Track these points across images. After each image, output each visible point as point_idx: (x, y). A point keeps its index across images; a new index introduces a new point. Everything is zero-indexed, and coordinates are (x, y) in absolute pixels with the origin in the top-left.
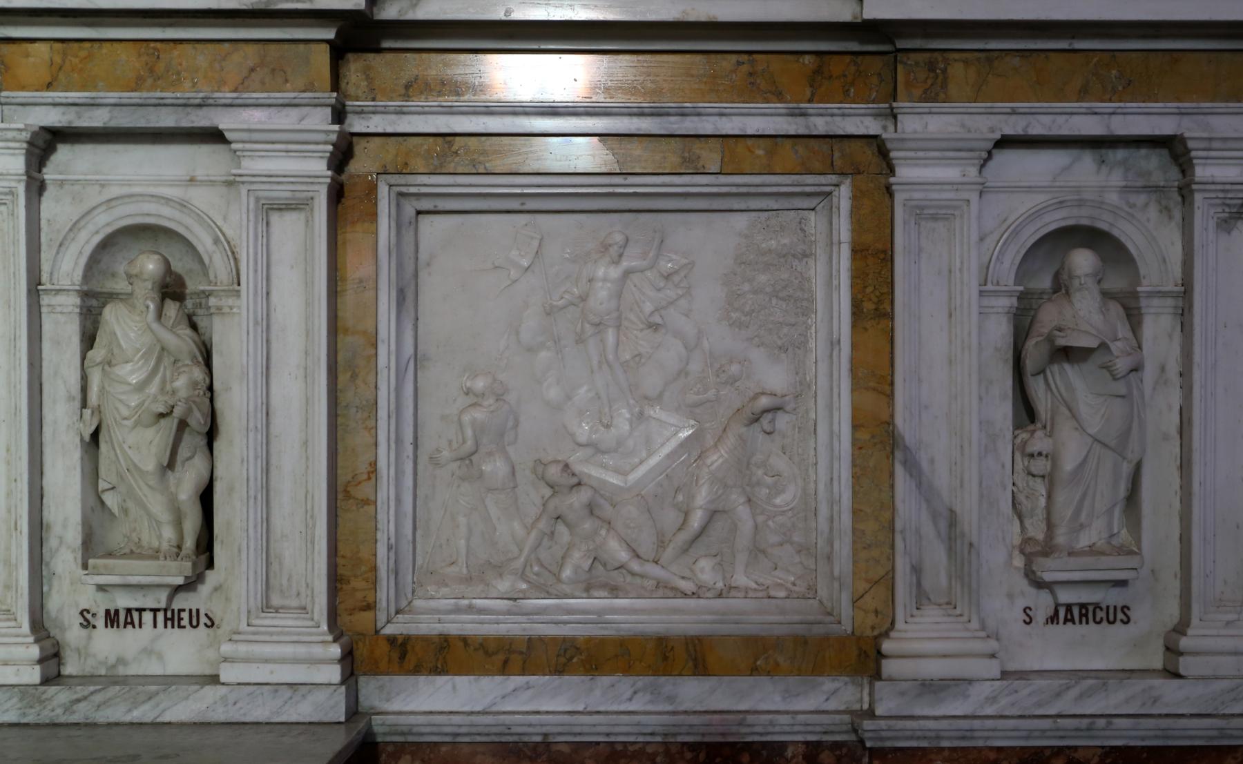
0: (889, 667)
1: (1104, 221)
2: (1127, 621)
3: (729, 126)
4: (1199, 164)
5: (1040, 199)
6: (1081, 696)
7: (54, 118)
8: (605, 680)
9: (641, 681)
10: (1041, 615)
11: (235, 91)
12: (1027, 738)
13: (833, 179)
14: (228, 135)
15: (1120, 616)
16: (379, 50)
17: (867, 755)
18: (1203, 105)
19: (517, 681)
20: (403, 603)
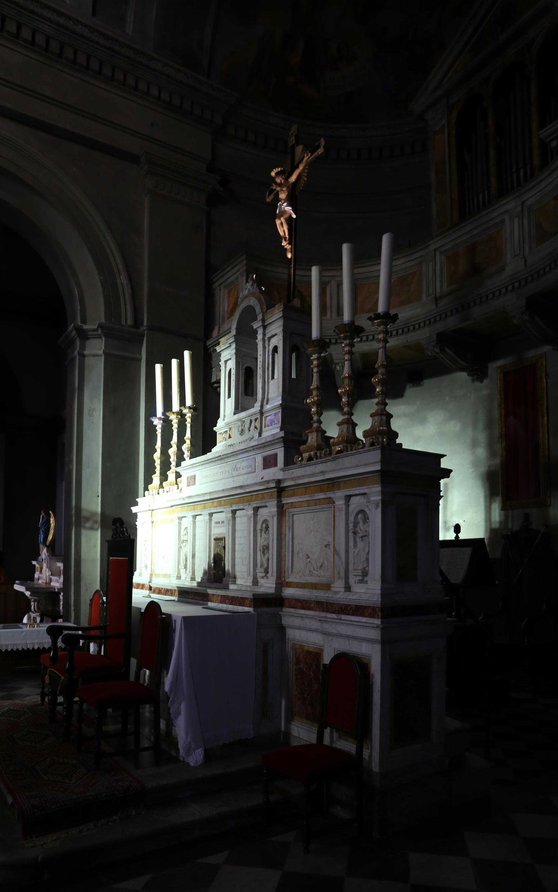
0: (332, 589)
1: (369, 508)
2: (367, 584)
3: (319, 497)
4: (292, 505)
5: (356, 505)
6: (353, 595)
7: (258, 505)
8: (306, 590)
9: (309, 590)
10: (357, 582)
11: (261, 500)
12: (344, 602)
13: (332, 504)
14: (268, 506)
15: (366, 583)
16: (285, 490)
17: (52, 515)
18: (370, 486)
19: (297, 589)
20: (289, 577)
